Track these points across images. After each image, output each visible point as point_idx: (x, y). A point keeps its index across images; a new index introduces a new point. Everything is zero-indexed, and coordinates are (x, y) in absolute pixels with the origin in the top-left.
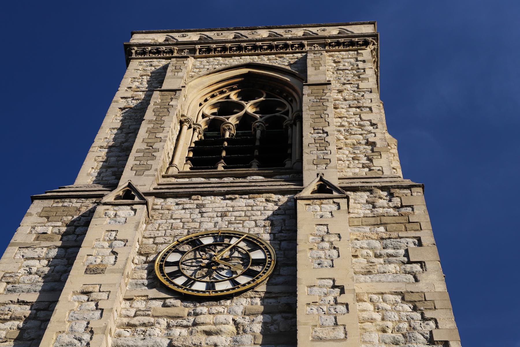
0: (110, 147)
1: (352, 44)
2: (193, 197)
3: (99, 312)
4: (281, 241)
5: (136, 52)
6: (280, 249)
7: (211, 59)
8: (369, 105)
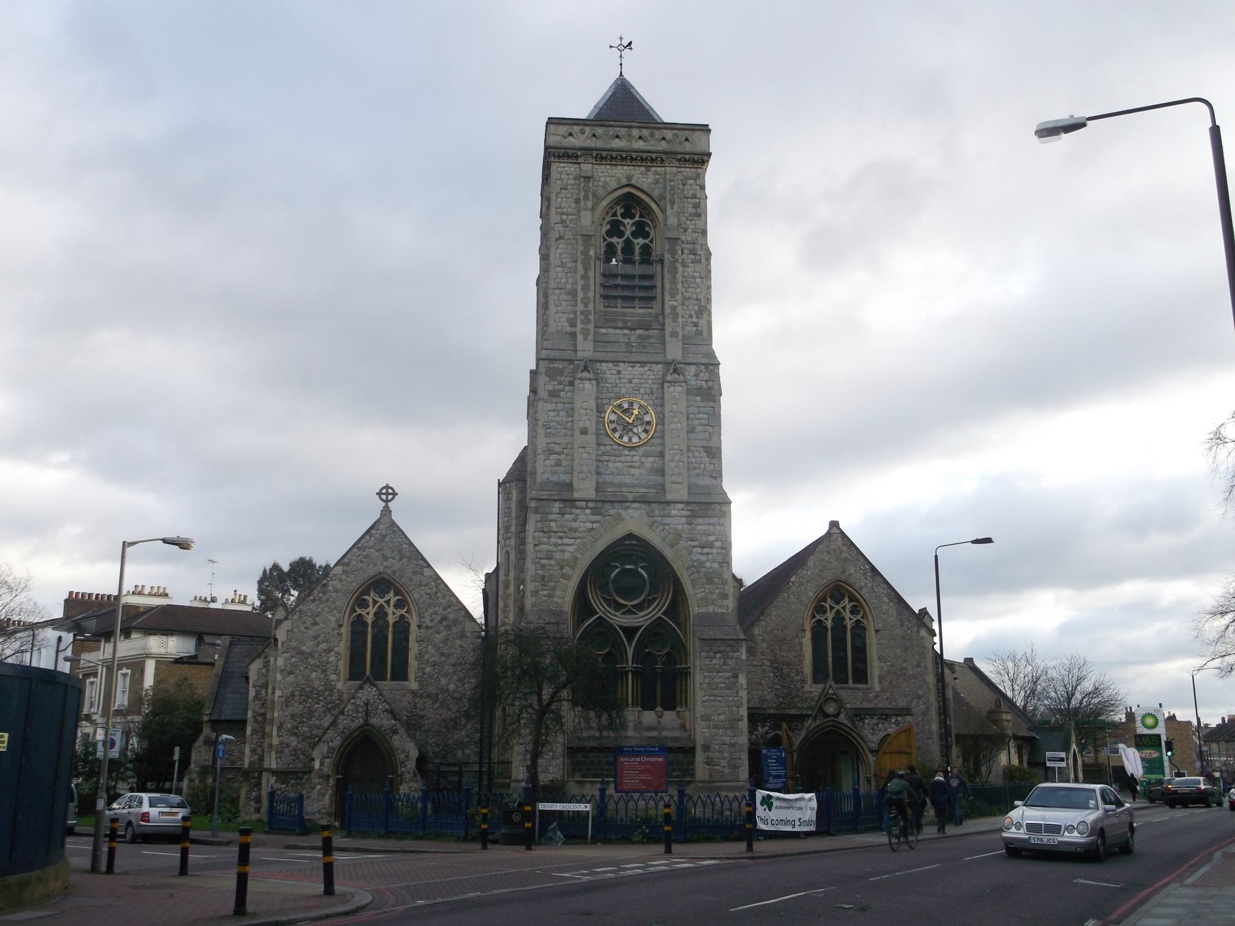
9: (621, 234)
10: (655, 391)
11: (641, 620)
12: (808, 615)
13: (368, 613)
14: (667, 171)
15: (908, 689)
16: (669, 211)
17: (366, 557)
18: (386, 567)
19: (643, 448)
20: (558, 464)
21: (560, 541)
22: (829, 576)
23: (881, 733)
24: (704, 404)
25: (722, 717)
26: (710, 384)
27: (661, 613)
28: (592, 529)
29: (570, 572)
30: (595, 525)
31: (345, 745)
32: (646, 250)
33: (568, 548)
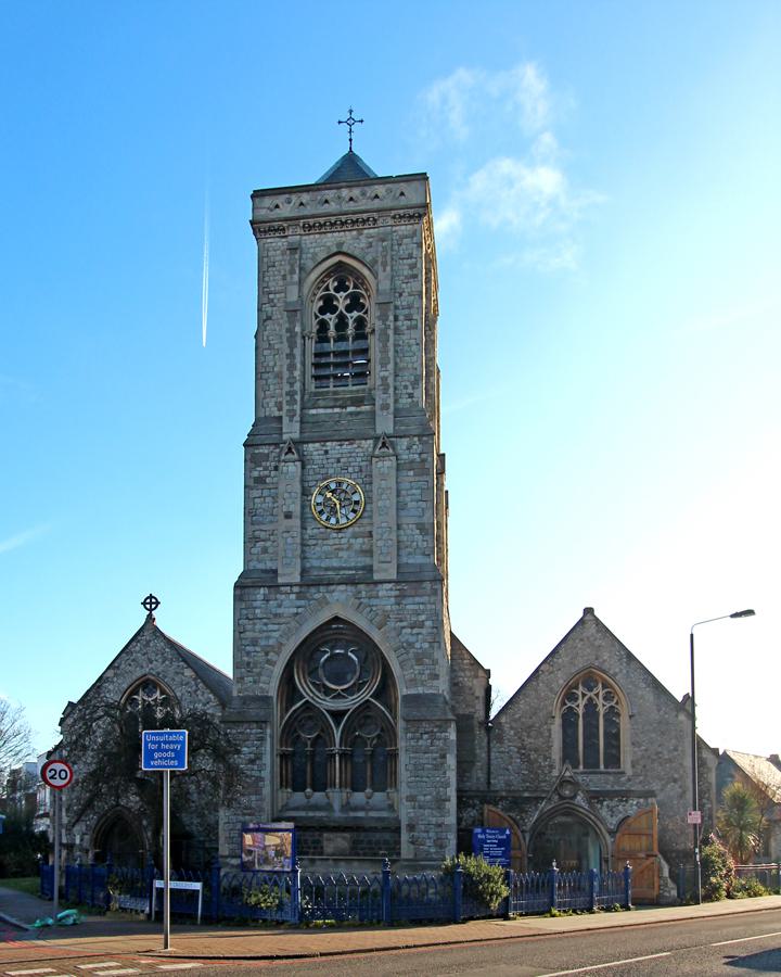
9: (333, 309)
10: (364, 469)
11: (349, 703)
12: (557, 701)
13: (578, 706)
16: (381, 275)
17: (133, 660)
18: (152, 669)
19: (351, 529)
20: (265, 550)
21: (265, 628)
22: (580, 663)
24: (417, 478)
25: (428, 797)
26: (424, 456)
28: (297, 614)
30: (300, 610)
31: (101, 822)
32: (360, 322)
33: (274, 634)
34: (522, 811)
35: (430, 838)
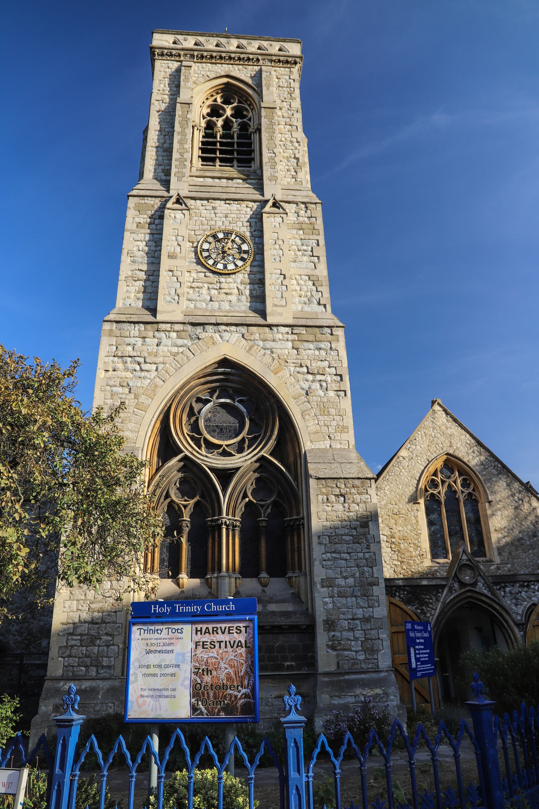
0: (157, 147)
1: (287, 62)
2: (210, 201)
3: (179, 283)
4: (255, 237)
5: (158, 53)
6: (255, 243)
7: (204, 64)
8: (296, 124)
14: (263, 69)
15: (527, 560)
23: (526, 603)
25: (351, 581)
27: (263, 451)
29: (148, 401)
30: (181, 349)
34: (422, 603)
35: (356, 639)
